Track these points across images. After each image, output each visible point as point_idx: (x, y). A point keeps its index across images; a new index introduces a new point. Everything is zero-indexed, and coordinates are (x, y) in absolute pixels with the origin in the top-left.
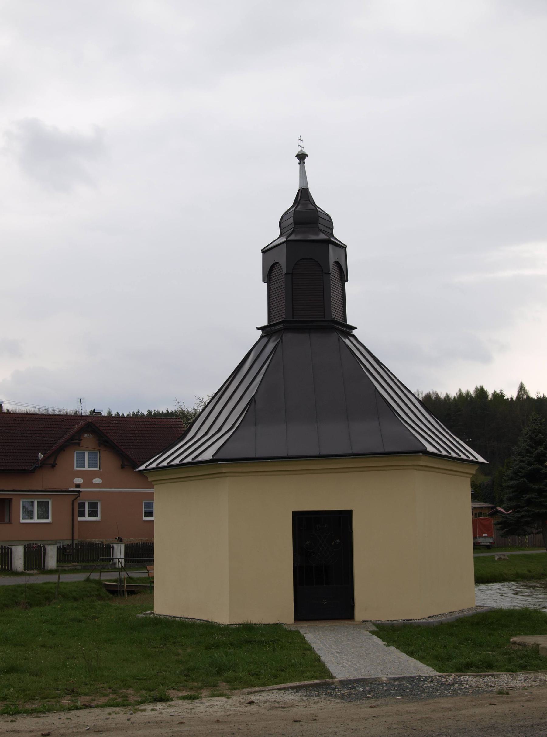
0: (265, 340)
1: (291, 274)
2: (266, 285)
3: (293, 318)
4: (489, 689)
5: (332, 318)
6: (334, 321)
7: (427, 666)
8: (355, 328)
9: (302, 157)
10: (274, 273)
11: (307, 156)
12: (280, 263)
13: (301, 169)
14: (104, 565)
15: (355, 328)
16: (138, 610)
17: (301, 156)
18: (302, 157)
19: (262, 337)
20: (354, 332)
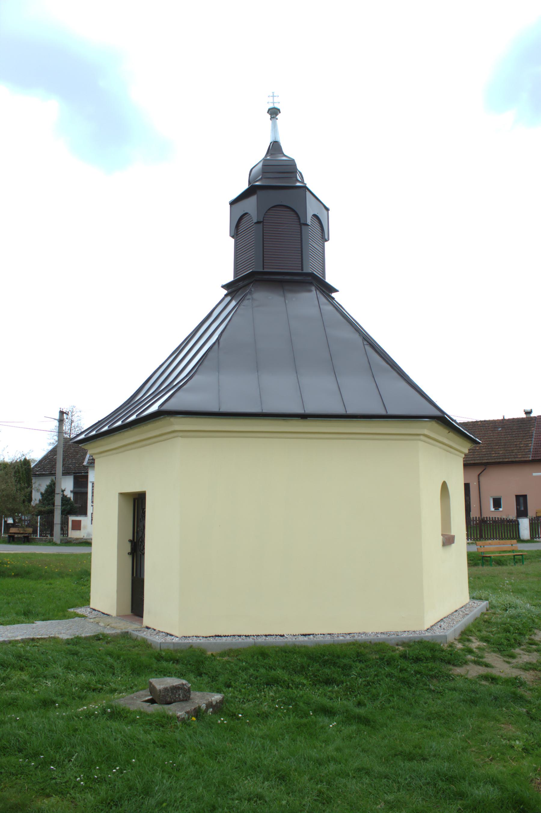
0: (229, 298)
1: (262, 224)
2: (233, 240)
3: (263, 269)
4: (297, 775)
5: (109, 639)
6: (312, 275)
7: (80, 636)
8: (336, 291)
9: (274, 112)
10: (242, 227)
11: (280, 112)
12: (250, 213)
13: (140, 534)
14: (114, 669)
15: (336, 291)
16: (218, 793)
17: (274, 110)
18: (274, 112)
19: (226, 296)
20: (334, 295)
